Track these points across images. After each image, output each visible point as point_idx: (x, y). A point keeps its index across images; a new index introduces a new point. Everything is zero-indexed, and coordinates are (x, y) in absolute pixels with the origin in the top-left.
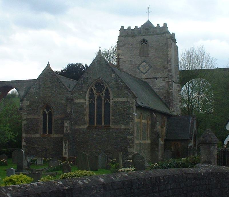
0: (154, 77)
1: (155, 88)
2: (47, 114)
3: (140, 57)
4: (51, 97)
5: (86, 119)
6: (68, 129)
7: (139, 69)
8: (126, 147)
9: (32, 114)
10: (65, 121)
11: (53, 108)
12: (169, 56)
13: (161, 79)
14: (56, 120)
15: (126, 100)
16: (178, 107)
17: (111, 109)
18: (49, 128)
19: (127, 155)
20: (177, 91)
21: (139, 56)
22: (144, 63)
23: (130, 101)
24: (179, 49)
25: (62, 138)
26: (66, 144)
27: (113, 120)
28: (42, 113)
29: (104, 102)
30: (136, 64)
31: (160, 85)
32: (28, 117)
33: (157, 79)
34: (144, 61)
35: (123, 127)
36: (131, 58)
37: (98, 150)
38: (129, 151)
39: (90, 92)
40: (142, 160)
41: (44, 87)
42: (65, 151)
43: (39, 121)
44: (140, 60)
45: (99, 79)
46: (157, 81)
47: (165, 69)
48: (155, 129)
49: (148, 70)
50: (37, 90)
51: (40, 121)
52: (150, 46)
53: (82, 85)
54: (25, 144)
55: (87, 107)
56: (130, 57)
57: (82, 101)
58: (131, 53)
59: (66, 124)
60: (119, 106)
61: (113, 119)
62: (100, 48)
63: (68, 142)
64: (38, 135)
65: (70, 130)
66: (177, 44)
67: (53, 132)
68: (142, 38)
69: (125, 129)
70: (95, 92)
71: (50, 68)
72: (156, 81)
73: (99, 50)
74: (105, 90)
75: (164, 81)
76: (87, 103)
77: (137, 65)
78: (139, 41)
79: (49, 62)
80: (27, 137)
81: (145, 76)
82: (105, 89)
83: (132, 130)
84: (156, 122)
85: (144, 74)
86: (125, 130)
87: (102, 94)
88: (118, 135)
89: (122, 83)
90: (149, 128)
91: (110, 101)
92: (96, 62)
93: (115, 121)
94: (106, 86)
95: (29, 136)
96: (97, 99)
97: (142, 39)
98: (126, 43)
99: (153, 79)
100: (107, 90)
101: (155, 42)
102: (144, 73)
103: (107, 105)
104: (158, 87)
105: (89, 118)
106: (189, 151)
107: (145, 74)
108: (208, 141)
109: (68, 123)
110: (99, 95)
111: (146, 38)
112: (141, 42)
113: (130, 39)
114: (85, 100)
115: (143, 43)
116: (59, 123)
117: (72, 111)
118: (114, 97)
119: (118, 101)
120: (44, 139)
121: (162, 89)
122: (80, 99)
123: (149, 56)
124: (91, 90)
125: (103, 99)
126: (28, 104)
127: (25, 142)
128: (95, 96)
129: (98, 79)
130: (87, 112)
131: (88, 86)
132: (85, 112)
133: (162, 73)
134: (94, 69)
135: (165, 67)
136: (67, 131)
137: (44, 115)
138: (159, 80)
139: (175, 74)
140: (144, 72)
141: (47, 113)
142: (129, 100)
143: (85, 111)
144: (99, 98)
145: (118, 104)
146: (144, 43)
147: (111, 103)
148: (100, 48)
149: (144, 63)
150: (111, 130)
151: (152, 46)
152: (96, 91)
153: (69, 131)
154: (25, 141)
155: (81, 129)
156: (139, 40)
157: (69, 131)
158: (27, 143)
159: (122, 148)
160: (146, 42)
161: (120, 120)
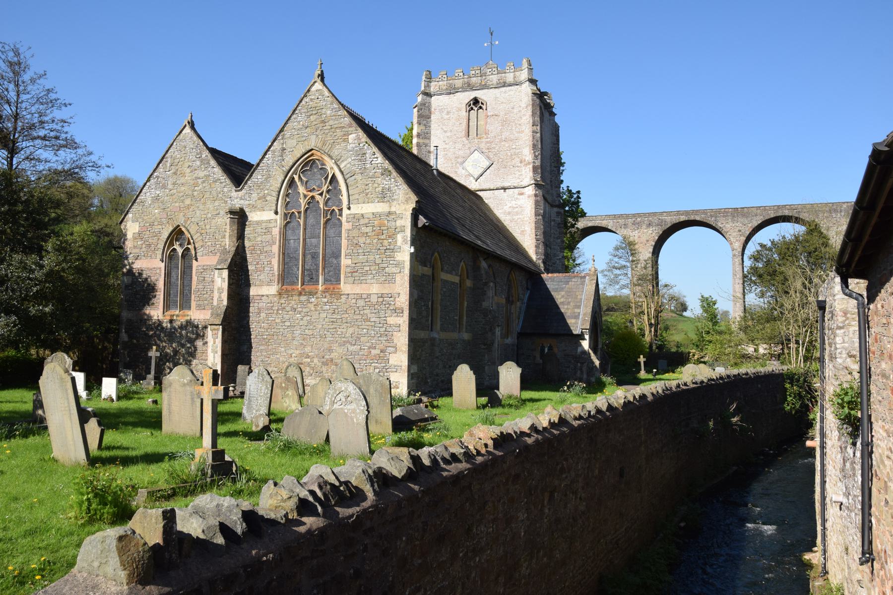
20: (556, 225)
21: (464, 139)
24: (560, 128)
27: (349, 270)
35: (375, 289)
36: (446, 144)
37: (306, 358)
42: (214, 357)
58: (445, 132)
60: (366, 225)
66: (557, 119)
77: (460, 160)
84: (486, 284)
86: (381, 299)
87: (321, 194)
88: (361, 312)
91: (341, 215)
93: (354, 272)
94: (332, 168)
97: (472, 97)
104: (510, 210)
108: (801, 238)
110: (313, 197)
139: (551, 186)
145: (362, 222)
147: (344, 219)
160: (480, 105)
161: (368, 268)
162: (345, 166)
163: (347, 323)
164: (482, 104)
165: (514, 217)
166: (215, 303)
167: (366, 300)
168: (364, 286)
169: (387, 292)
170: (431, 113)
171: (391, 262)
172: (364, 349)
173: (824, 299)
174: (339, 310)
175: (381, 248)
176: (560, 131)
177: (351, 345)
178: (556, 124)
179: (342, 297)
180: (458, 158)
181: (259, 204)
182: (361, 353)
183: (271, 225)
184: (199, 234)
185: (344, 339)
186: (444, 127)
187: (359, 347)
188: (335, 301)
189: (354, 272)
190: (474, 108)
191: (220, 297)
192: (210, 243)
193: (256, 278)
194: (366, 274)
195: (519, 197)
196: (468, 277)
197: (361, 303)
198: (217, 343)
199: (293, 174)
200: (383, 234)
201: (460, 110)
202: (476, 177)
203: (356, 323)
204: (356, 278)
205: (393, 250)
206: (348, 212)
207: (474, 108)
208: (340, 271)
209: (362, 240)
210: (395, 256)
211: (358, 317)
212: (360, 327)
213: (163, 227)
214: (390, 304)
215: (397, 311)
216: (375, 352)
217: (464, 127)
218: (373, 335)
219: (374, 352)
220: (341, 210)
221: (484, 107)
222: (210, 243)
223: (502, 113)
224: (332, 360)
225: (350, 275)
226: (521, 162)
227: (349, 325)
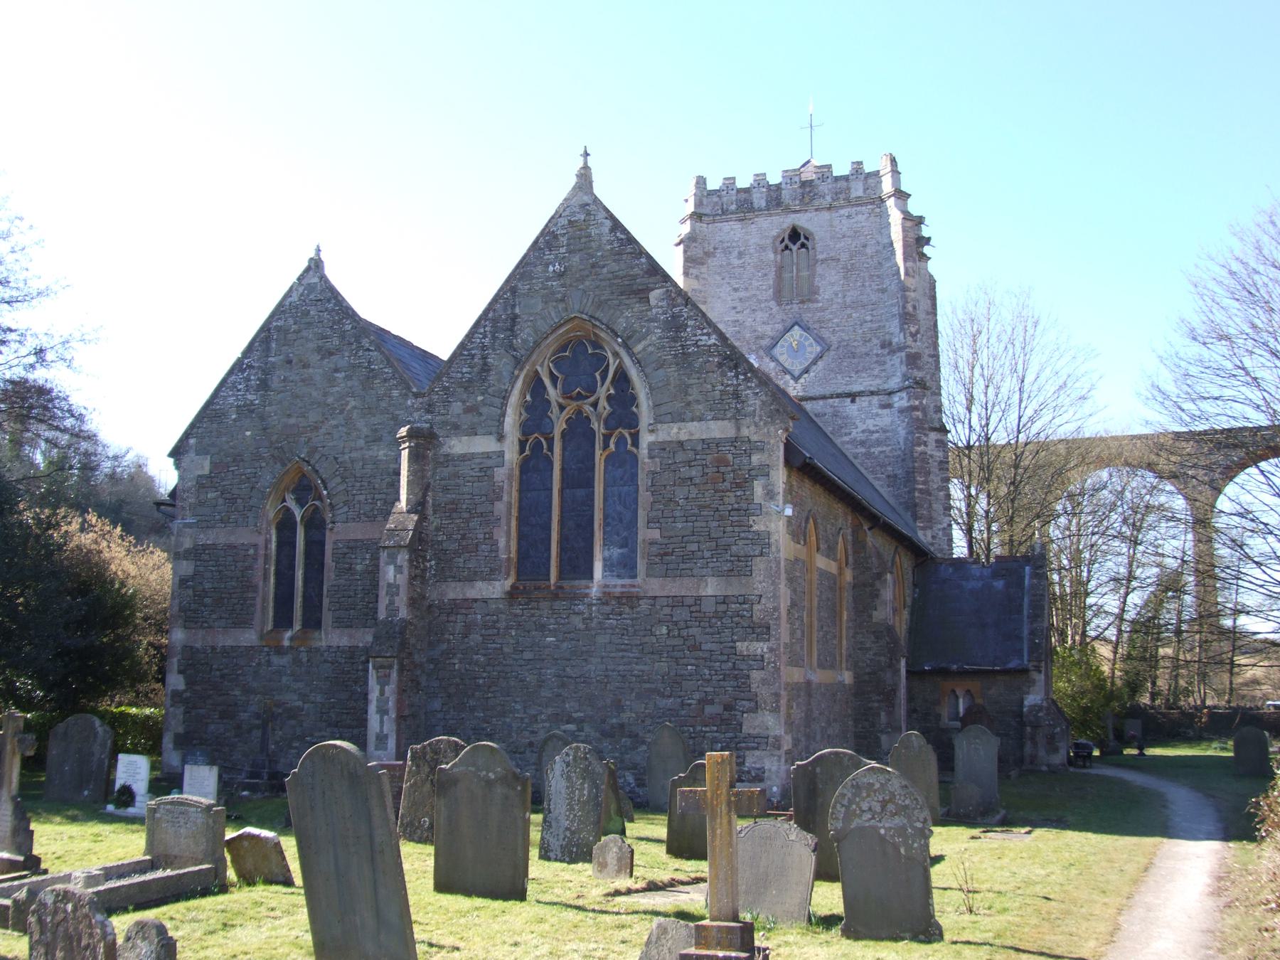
0: (839, 391)
1: (846, 439)
2: (298, 519)
3: (779, 304)
4: (323, 431)
5: (502, 543)
6: (402, 601)
7: (773, 359)
8: (728, 707)
9: (222, 521)
10: (384, 556)
11: (331, 485)
12: (907, 293)
13: (875, 400)
14: (345, 550)
15: (731, 433)
16: (940, 533)
17: (643, 480)
18: (304, 596)
21: (772, 304)
23: (754, 438)
25: (368, 653)
26: (383, 681)
27: (654, 549)
28: (271, 515)
29: (606, 446)
31: (870, 424)
32: (207, 538)
33: (857, 399)
34: (796, 323)
35: (711, 588)
36: (737, 312)
37: (568, 723)
39: (528, 398)
40: (898, 821)
41: (284, 380)
42: (382, 722)
43: (255, 559)
44: (779, 317)
45: (576, 322)
46: (854, 407)
47: (892, 352)
48: (875, 613)
49: (814, 362)
50: (250, 397)
51: (261, 561)
52: (820, 257)
53: (484, 358)
54: (182, 687)
55: (510, 477)
56: (735, 308)
57: (483, 444)
58: (736, 290)
59: (389, 574)
60: (689, 464)
61: (652, 543)
62: (586, 154)
63: (401, 670)
64: (248, 637)
65: (413, 603)
67: (327, 617)
68: (788, 221)
69: (725, 600)
70: (553, 394)
71: (323, 278)
72: (851, 409)
73: (581, 164)
74: (612, 382)
75: (888, 406)
76: (507, 457)
77: (766, 342)
78: (775, 238)
79: (318, 250)
80: (192, 647)
81: (799, 386)
83: (767, 604)
84: (879, 576)
85: (796, 379)
86: (722, 608)
88: (684, 633)
89: (708, 334)
90: (844, 603)
91: (636, 443)
92: (563, 227)
93: (666, 554)
94: (616, 355)
95: (200, 640)
96: (563, 434)
97: (785, 226)
98: (715, 249)
99: (837, 400)
100: (622, 378)
101: (844, 237)
102: (796, 374)
103: (624, 461)
104: (862, 437)
105: (521, 537)
106: (1029, 729)
107: (802, 380)
109: (399, 569)
110: (579, 412)
111: (803, 221)
112: (783, 241)
113: (731, 230)
114: (501, 437)
116: (359, 567)
117: (429, 499)
118: (658, 419)
119: (683, 437)
120: (276, 660)
121: (879, 443)
122: (473, 432)
123: (818, 302)
124: (536, 386)
125: (598, 427)
126: (206, 472)
127: (180, 672)
128: (553, 417)
129: (572, 319)
130: (510, 503)
131: (519, 363)
132: (500, 507)
133: (876, 372)
134: (551, 268)
135: (890, 344)
136: (392, 609)
137: (286, 525)
138: (862, 402)
140: (797, 368)
141: (298, 514)
143: (499, 498)
144: (579, 430)
145: (680, 457)
146: (794, 244)
147: (643, 451)
148: (586, 154)
150: (644, 606)
151: (832, 254)
152: (559, 385)
153: (403, 613)
154: (182, 668)
155: (475, 600)
156: (774, 233)
157: (403, 613)
158: (190, 683)
159: (709, 709)
160: (802, 240)
161: (694, 547)
162: (644, 349)
163: (652, 653)
164: (807, 238)
165: (873, 450)
166: (382, 615)
167: (693, 609)
168: (686, 581)
169: (736, 593)
171: (742, 535)
172: (690, 705)
174: (637, 627)
175: (721, 508)
176: (937, 290)
177: (663, 696)
178: (931, 276)
179: (641, 602)
181: (468, 419)
182: (683, 712)
183: (490, 463)
184: (338, 480)
185: (648, 686)
186: (733, 282)
187: (679, 700)
190: (791, 245)
191: (391, 603)
192: (362, 498)
193: (461, 565)
194: (691, 557)
195: (880, 411)
197: (681, 614)
198: (387, 693)
200: (724, 481)
203: (672, 654)
204: (671, 566)
205: (747, 513)
207: (791, 245)
209: (681, 493)
210: (751, 522)
212: (682, 661)
213: (264, 464)
217: (771, 282)
218: (708, 677)
219: (709, 709)
221: (809, 244)
222: (362, 498)
223: (844, 257)
224: (622, 726)
226: (883, 346)
227: (657, 657)
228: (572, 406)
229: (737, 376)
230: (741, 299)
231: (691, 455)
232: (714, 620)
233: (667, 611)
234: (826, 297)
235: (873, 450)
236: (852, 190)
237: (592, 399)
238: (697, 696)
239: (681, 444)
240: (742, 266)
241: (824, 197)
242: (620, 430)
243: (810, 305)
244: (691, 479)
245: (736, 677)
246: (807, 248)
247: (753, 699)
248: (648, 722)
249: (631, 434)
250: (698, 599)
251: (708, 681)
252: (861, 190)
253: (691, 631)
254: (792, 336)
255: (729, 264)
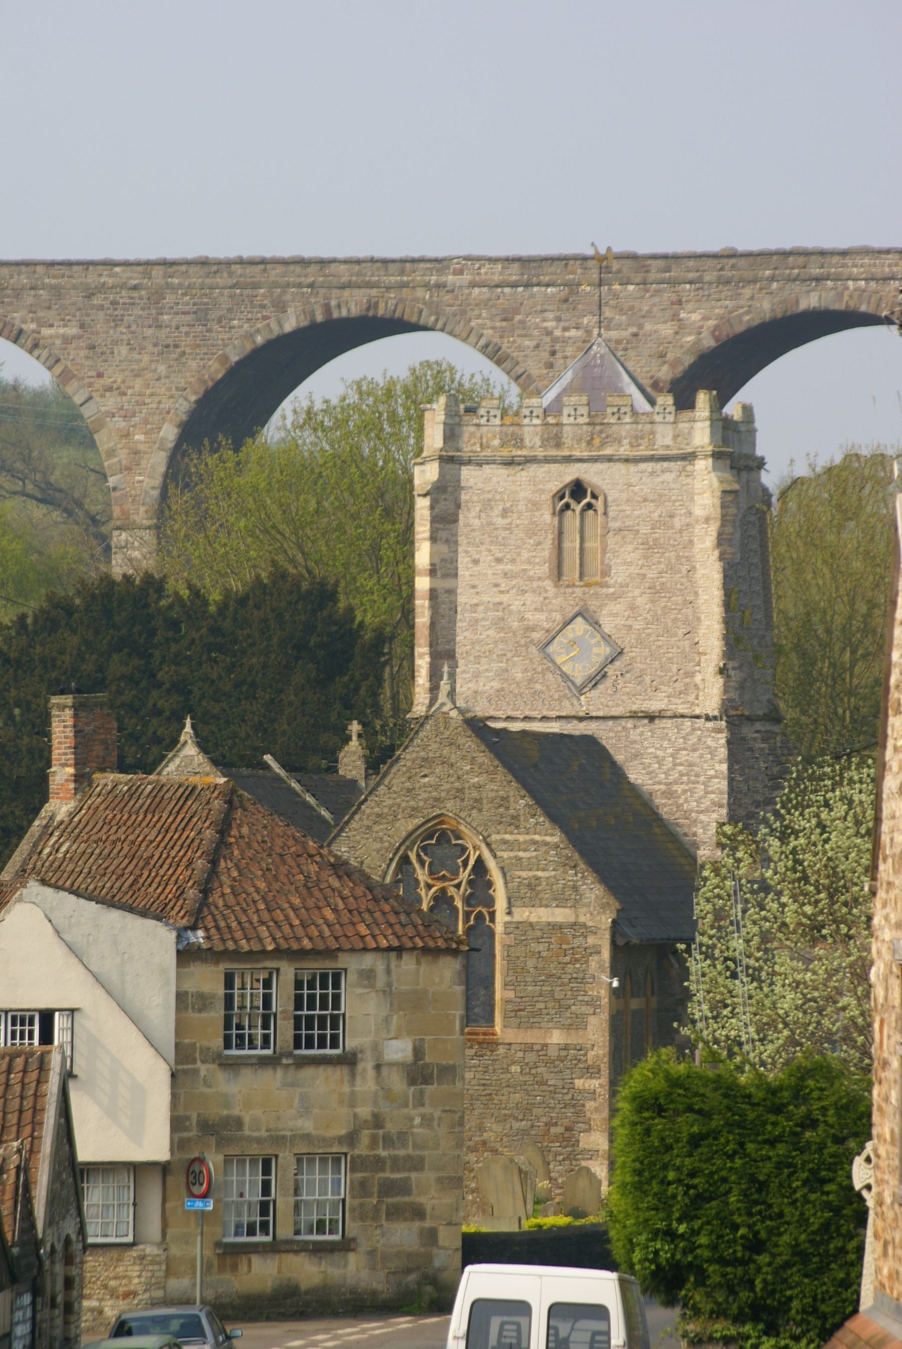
8: (568, 1129)
15: (572, 919)
19: (574, 1163)
21: (548, 584)
22: (580, 625)
23: (590, 924)
27: (510, 1007)
30: (533, 629)
35: (556, 1037)
36: (502, 592)
38: (582, 1145)
56: (497, 585)
58: (499, 560)
60: (538, 940)
68: (571, 473)
69: (566, 1047)
82: (470, 867)
86: (564, 1053)
87: (458, 886)
88: (534, 1071)
91: (492, 920)
93: (520, 1010)
97: (568, 479)
100: (480, 867)
110: (443, 890)
111: (591, 474)
115: (571, 501)
119: (533, 919)
123: (608, 586)
142: (582, 919)
147: (499, 928)
149: (580, 625)
150: (501, 1050)
159: (553, 1130)
161: (542, 1006)
164: (594, 496)
169: (575, 1042)
170: (458, 506)
173: (441, 1243)
177: (516, 1119)
180: (533, 629)
188: (489, 1053)
189: (520, 1010)
190: (573, 504)
194: (540, 1013)
196: (653, 994)
199: (406, 850)
201: (535, 506)
202: (579, 681)
206: (508, 918)
208: (492, 1007)
211: (527, 1078)
214: (579, 1060)
215: (591, 1071)
216: (559, 1130)
217: (546, 553)
220: (492, 915)
221: (599, 504)
224: (484, 1143)
225: (512, 1014)
227: (512, 1090)
228: (438, 885)
229: (576, 874)
230: (506, 574)
231: (539, 933)
232: (557, 1063)
233: (520, 1054)
234: (619, 580)
235: (674, 788)
236: (658, 436)
237: (456, 882)
238: (545, 1119)
239: (531, 924)
240: (508, 528)
241: (620, 442)
242: (479, 909)
243: (598, 589)
244: (539, 952)
245: (574, 1106)
246: (595, 511)
247: (588, 1122)
248: (505, 1139)
249: (489, 912)
250: (545, 1046)
251: (553, 1108)
252: (670, 437)
253: (539, 1070)
254: (573, 630)
255: (490, 524)
